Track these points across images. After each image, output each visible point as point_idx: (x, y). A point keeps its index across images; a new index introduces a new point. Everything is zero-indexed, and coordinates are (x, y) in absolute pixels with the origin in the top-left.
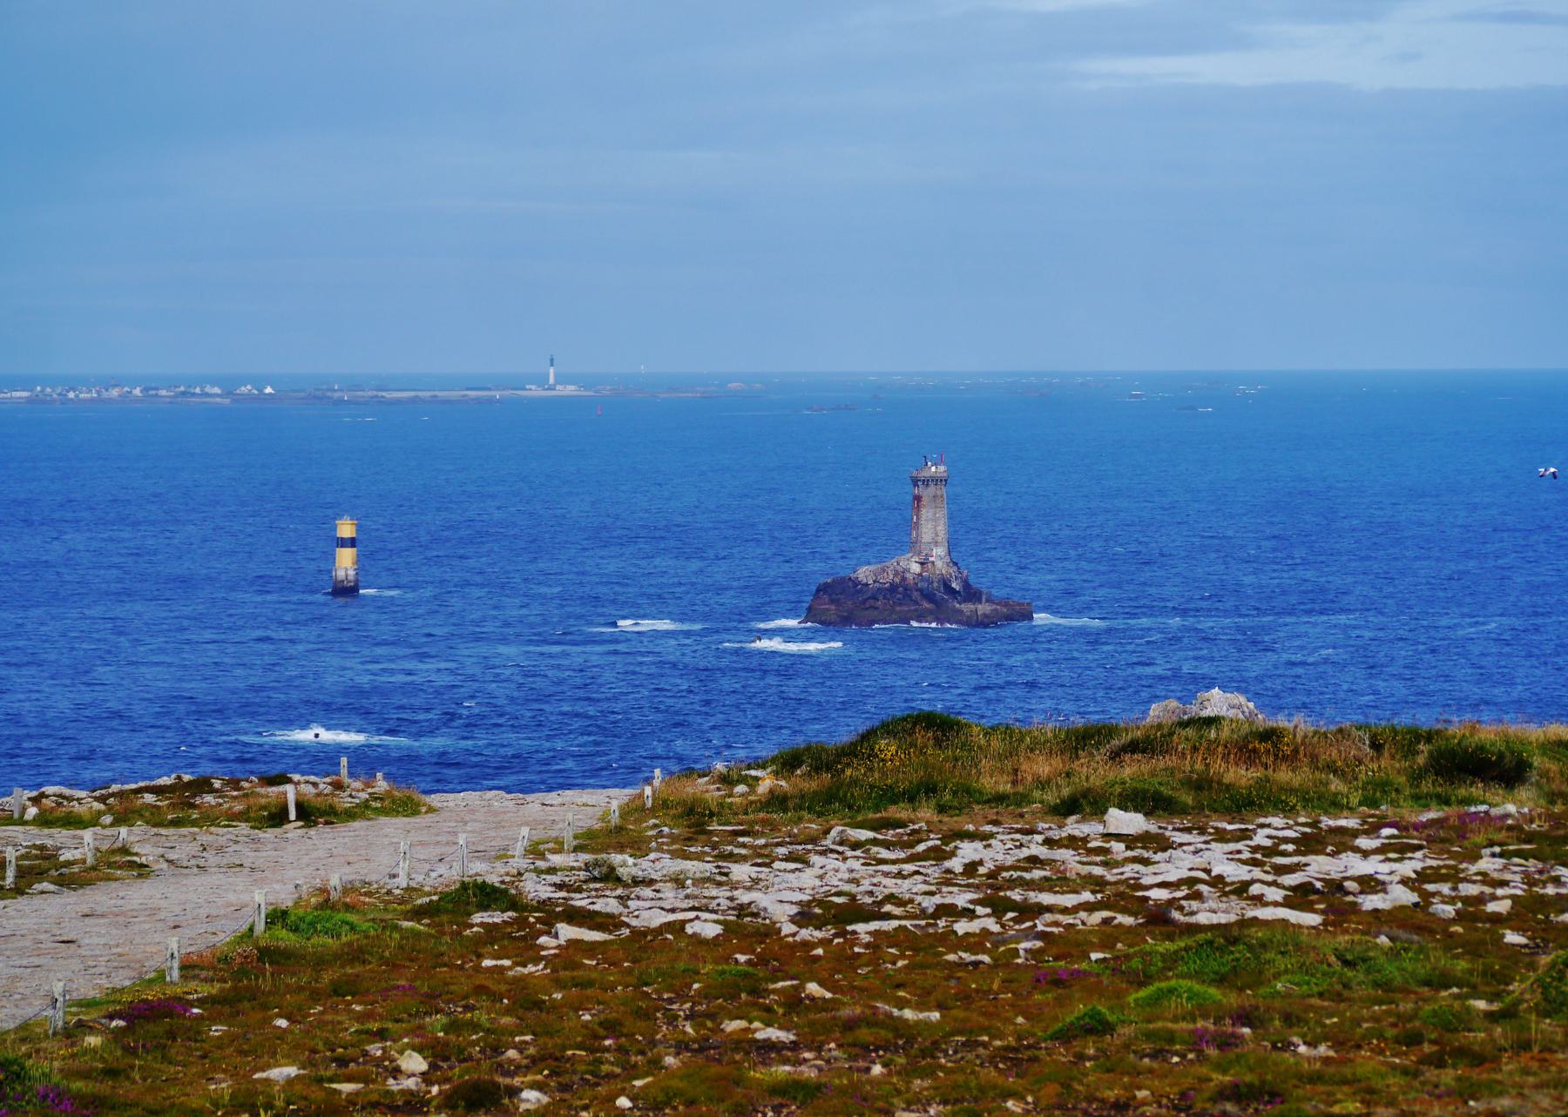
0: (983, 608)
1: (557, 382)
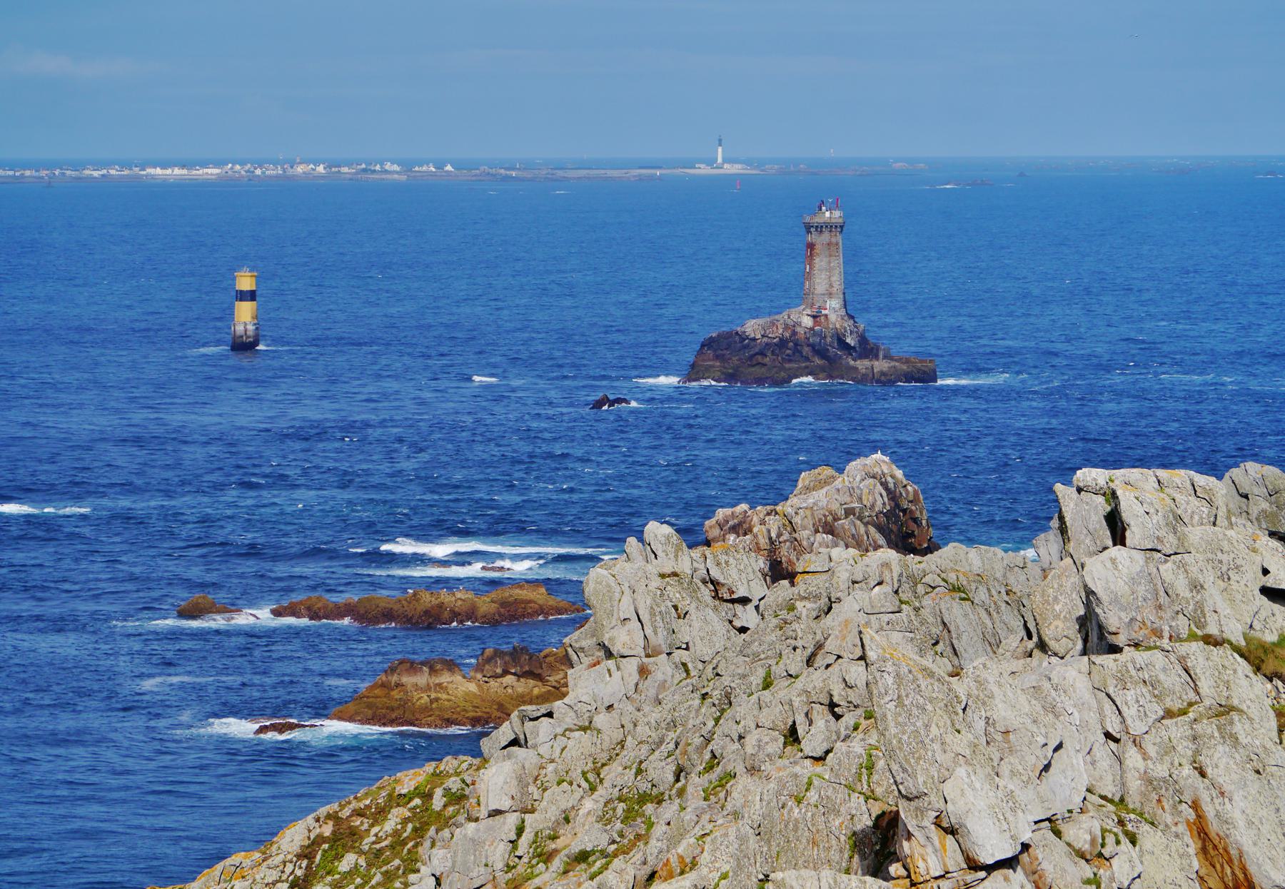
0: (880, 365)
1: (725, 161)
